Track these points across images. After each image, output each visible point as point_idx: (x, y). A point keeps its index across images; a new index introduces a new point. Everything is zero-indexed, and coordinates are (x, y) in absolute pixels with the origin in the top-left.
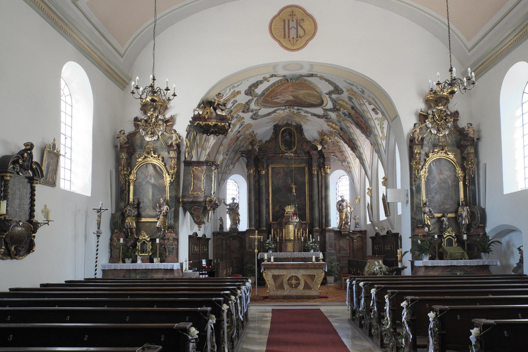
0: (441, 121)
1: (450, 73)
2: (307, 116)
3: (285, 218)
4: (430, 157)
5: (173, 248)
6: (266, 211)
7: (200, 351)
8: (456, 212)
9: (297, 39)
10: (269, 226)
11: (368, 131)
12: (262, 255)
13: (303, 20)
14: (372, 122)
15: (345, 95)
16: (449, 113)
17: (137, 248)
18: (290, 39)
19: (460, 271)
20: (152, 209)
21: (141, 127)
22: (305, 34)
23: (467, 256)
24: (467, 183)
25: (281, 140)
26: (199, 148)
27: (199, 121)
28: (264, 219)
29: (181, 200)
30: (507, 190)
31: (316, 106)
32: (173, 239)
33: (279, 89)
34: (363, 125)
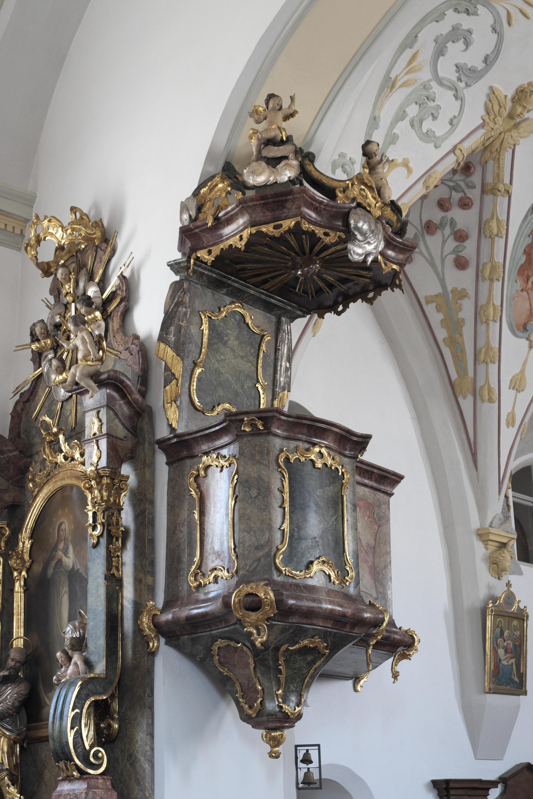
7: (6, 434)
26: (465, 397)
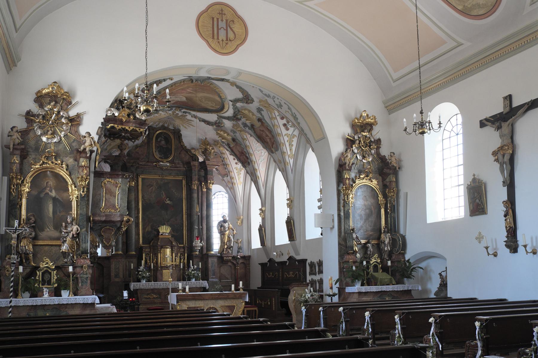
0: (366, 147)
1: (421, 115)
2: (193, 121)
3: (159, 241)
4: (357, 183)
5: (87, 277)
6: (136, 232)
8: (379, 238)
9: (226, 42)
10: (140, 250)
11: (274, 147)
12: (135, 285)
13: (233, 21)
14: (282, 138)
15: (253, 107)
16: (373, 140)
17: (37, 278)
18: (219, 41)
19: (388, 296)
20: (53, 229)
21: (37, 124)
22: (235, 38)
23: (394, 282)
24: (388, 211)
25: (156, 146)
27: (114, 124)
28: (134, 241)
29: (92, 219)
30: (431, 219)
31: (211, 112)
32: (88, 266)
33: (177, 88)
34: (268, 140)
